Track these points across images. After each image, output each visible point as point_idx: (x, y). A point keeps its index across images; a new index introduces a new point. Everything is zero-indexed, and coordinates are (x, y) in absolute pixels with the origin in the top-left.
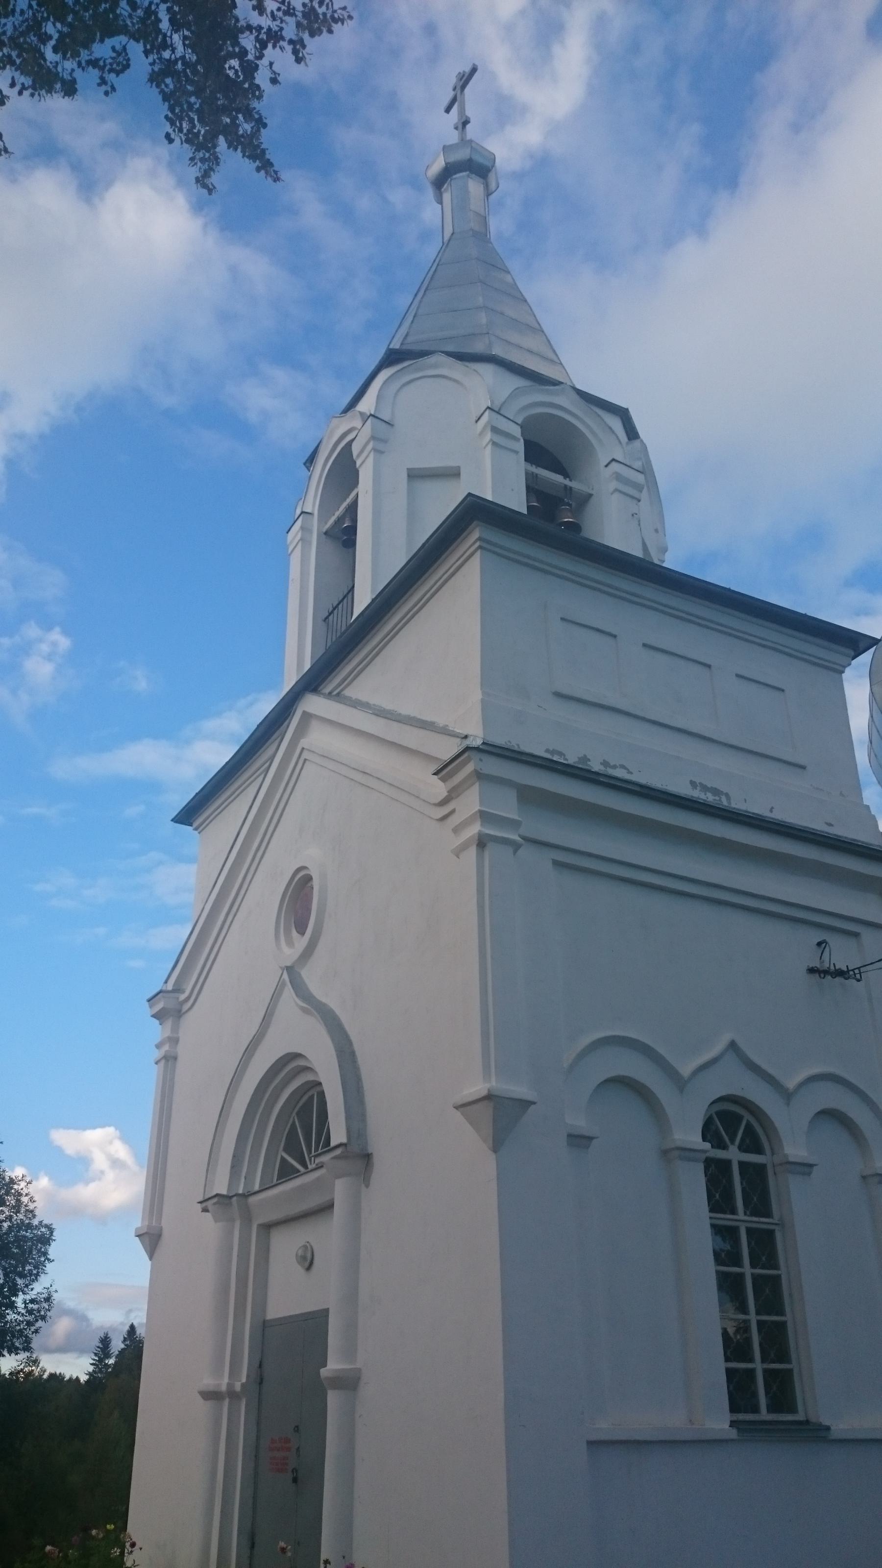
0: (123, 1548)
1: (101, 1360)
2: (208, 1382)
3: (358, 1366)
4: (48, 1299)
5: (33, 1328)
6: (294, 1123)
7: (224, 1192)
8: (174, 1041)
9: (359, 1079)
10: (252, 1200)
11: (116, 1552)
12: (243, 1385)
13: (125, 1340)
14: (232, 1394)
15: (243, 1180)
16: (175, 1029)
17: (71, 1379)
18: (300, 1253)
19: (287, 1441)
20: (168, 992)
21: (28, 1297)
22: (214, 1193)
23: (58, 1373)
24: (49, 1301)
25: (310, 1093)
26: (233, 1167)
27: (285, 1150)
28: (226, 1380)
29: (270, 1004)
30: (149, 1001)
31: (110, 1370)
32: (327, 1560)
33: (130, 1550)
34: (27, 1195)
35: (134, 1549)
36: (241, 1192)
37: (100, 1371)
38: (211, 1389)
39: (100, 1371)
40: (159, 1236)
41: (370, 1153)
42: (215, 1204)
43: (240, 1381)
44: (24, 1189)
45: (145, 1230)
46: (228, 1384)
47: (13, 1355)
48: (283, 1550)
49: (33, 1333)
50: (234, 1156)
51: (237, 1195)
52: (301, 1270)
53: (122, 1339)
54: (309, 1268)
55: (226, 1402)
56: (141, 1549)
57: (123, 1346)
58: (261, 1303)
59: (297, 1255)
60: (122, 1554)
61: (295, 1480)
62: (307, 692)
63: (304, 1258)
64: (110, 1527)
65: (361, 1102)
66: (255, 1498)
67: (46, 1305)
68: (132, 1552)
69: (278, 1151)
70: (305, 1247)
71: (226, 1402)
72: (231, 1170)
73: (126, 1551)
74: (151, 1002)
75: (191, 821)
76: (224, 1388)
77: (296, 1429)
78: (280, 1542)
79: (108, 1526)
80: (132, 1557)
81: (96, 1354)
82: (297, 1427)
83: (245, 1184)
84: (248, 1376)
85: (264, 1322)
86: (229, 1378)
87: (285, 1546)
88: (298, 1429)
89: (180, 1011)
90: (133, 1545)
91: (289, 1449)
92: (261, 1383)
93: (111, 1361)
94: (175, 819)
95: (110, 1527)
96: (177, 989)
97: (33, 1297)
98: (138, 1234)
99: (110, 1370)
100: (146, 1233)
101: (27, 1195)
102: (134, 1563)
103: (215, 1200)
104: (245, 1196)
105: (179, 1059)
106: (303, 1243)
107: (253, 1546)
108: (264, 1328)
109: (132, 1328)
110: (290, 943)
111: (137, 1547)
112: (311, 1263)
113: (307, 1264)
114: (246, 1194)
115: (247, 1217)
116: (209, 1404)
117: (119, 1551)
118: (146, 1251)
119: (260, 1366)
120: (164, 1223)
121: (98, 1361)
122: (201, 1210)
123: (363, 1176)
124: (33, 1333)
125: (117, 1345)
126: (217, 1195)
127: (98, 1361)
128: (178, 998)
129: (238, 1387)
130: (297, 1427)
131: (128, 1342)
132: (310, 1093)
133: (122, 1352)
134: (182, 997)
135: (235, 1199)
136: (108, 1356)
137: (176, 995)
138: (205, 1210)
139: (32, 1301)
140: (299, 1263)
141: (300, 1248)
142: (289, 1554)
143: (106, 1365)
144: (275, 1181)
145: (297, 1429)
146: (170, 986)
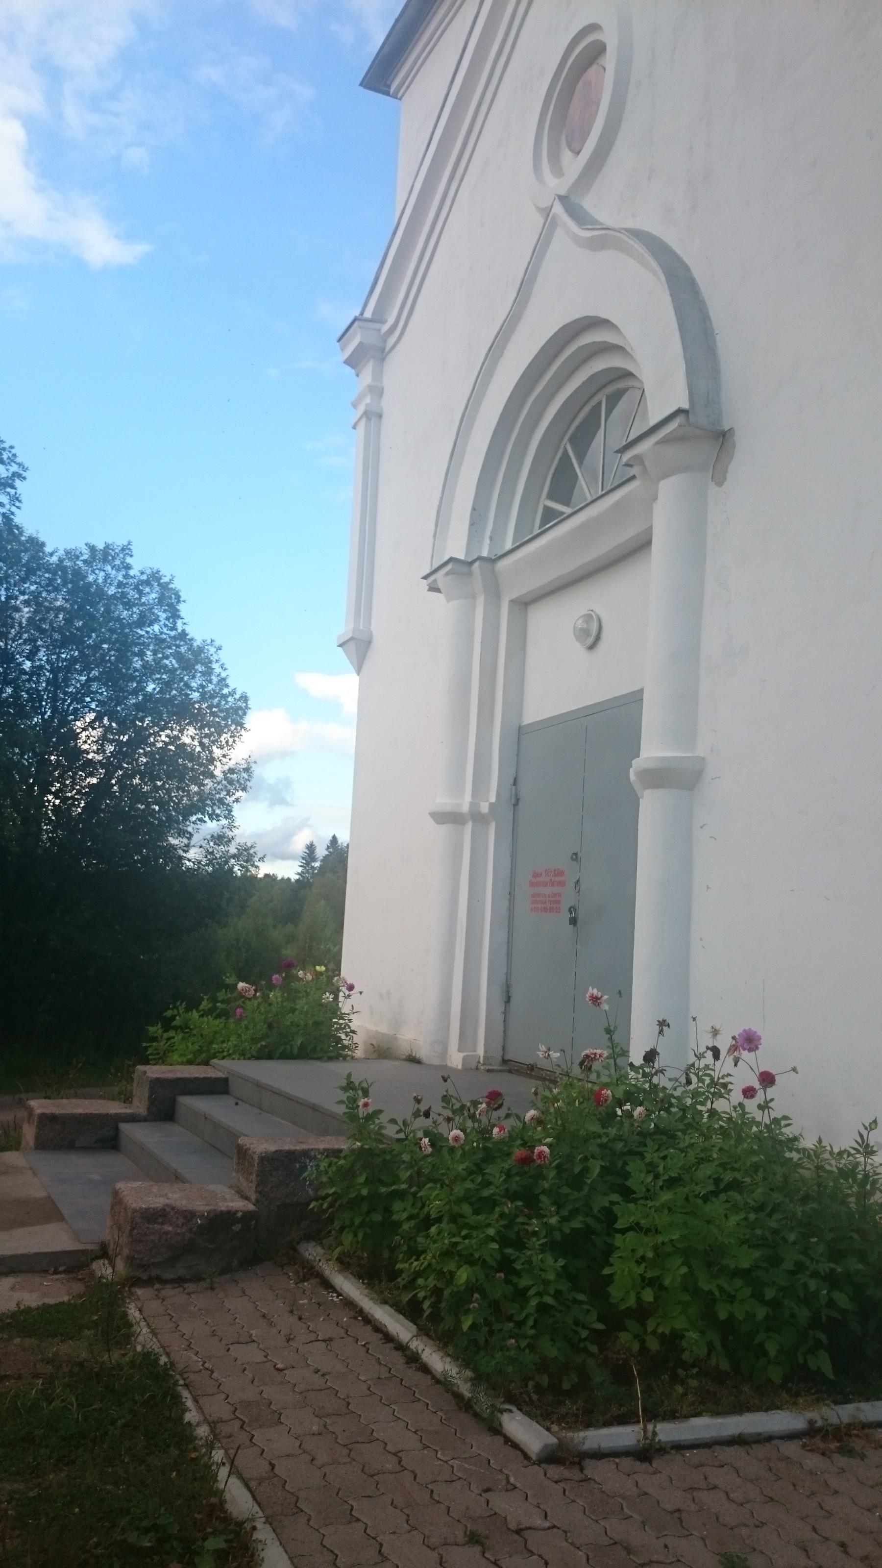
0: (336, 993)
1: (308, 864)
2: (443, 801)
3: (700, 752)
4: (247, 770)
5: (233, 798)
6: (565, 452)
7: (462, 557)
8: (377, 391)
9: (705, 318)
10: (501, 565)
11: (328, 998)
12: (491, 805)
13: (328, 847)
14: (477, 817)
15: (487, 541)
16: (378, 374)
17: (283, 879)
18: (580, 624)
19: (560, 873)
20: (366, 320)
21: (226, 768)
22: (446, 558)
23: (271, 874)
24: (248, 772)
25: (593, 402)
26: (472, 524)
27: (571, 440)
28: (468, 799)
29: (529, 263)
30: (339, 340)
31: (316, 871)
32: (664, 1021)
33: (347, 993)
34: (217, 661)
35: (351, 993)
36: (485, 554)
37: (308, 872)
38: (448, 809)
39: (308, 872)
40: (369, 643)
41: (727, 428)
42: (447, 574)
43: (487, 801)
44: (214, 655)
45: (350, 635)
46: (472, 805)
47: (214, 821)
48: (595, 1000)
49: (234, 802)
50: (474, 509)
51: (479, 558)
52: (579, 649)
53: (326, 847)
54: (592, 647)
55: (469, 827)
56: (361, 993)
57: (327, 853)
58: (515, 701)
59: (575, 627)
60: (336, 998)
61: (573, 922)
62: (229, 1507)
63: (585, 632)
64: (321, 969)
65: (711, 350)
66: (509, 942)
67: (245, 775)
68: (349, 996)
69: (539, 498)
70: (588, 618)
71: (469, 827)
72: (470, 528)
73: (341, 994)
74: (341, 342)
75: (388, 82)
76: (465, 808)
77: (574, 857)
78: (590, 988)
79: (318, 968)
80: (349, 1002)
81: (303, 858)
82: (576, 854)
83: (491, 546)
84: (498, 795)
85: (520, 728)
86: (472, 795)
87: (600, 994)
88: (577, 857)
89: (383, 350)
90: (351, 988)
91: (562, 884)
92: (516, 805)
93: (317, 864)
94: (364, 84)
95: (321, 969)
96: (378, 318)
97: (232, 767)
98: (341, 642)
99: (316, 871)
100: (351, 639)
101: (217, 661)
102: (353, 1009)
103: (449, 567)
104: (493, 561)
105: (385, 417)
106: (586, 612)
107: (508, 1000)
108: (521, 732)
109: (334, 839)
110: (558, 170)
111: (355, 990)
112: (598, 638)
113: (591, 640)
114: (493, 558)
115: (494, 593)
116: (443, 830)
117: (332, 996)
118: (351, 662)
119: (515, 783)
120: (374, 628)
121: (306, 864)
122: (427, 587)
123: (711, 471)
124: (234, 802)
125: (321, 852)
126: (451, 559)
127: (306, 864)
128: (379, 330)
129: (485, 808)
130: (576, 854)
131: (331, 850)
132: (593, 402)
133: (326, 858)
134: (385, 328)
135: (477, 564)
136: (314, 859)
137: (376, 326)
138: (434, 588)
139: (232, 771)
140: (578, 638)
141: (581, 617)
142: (606, 1007)
143: (313, 867)
144: (537, 531)
145: (575, 857)
146: (368, 314)
